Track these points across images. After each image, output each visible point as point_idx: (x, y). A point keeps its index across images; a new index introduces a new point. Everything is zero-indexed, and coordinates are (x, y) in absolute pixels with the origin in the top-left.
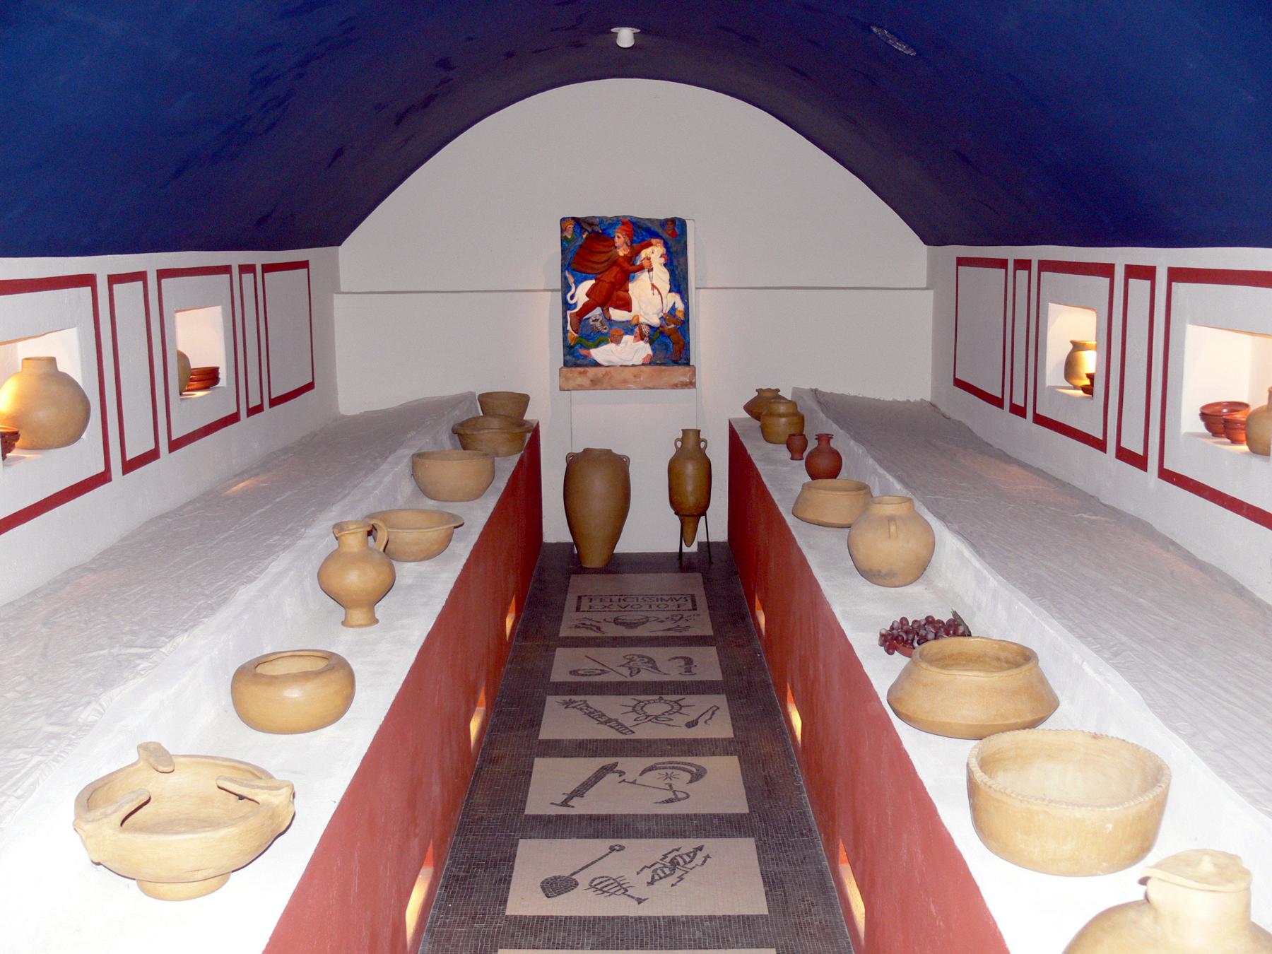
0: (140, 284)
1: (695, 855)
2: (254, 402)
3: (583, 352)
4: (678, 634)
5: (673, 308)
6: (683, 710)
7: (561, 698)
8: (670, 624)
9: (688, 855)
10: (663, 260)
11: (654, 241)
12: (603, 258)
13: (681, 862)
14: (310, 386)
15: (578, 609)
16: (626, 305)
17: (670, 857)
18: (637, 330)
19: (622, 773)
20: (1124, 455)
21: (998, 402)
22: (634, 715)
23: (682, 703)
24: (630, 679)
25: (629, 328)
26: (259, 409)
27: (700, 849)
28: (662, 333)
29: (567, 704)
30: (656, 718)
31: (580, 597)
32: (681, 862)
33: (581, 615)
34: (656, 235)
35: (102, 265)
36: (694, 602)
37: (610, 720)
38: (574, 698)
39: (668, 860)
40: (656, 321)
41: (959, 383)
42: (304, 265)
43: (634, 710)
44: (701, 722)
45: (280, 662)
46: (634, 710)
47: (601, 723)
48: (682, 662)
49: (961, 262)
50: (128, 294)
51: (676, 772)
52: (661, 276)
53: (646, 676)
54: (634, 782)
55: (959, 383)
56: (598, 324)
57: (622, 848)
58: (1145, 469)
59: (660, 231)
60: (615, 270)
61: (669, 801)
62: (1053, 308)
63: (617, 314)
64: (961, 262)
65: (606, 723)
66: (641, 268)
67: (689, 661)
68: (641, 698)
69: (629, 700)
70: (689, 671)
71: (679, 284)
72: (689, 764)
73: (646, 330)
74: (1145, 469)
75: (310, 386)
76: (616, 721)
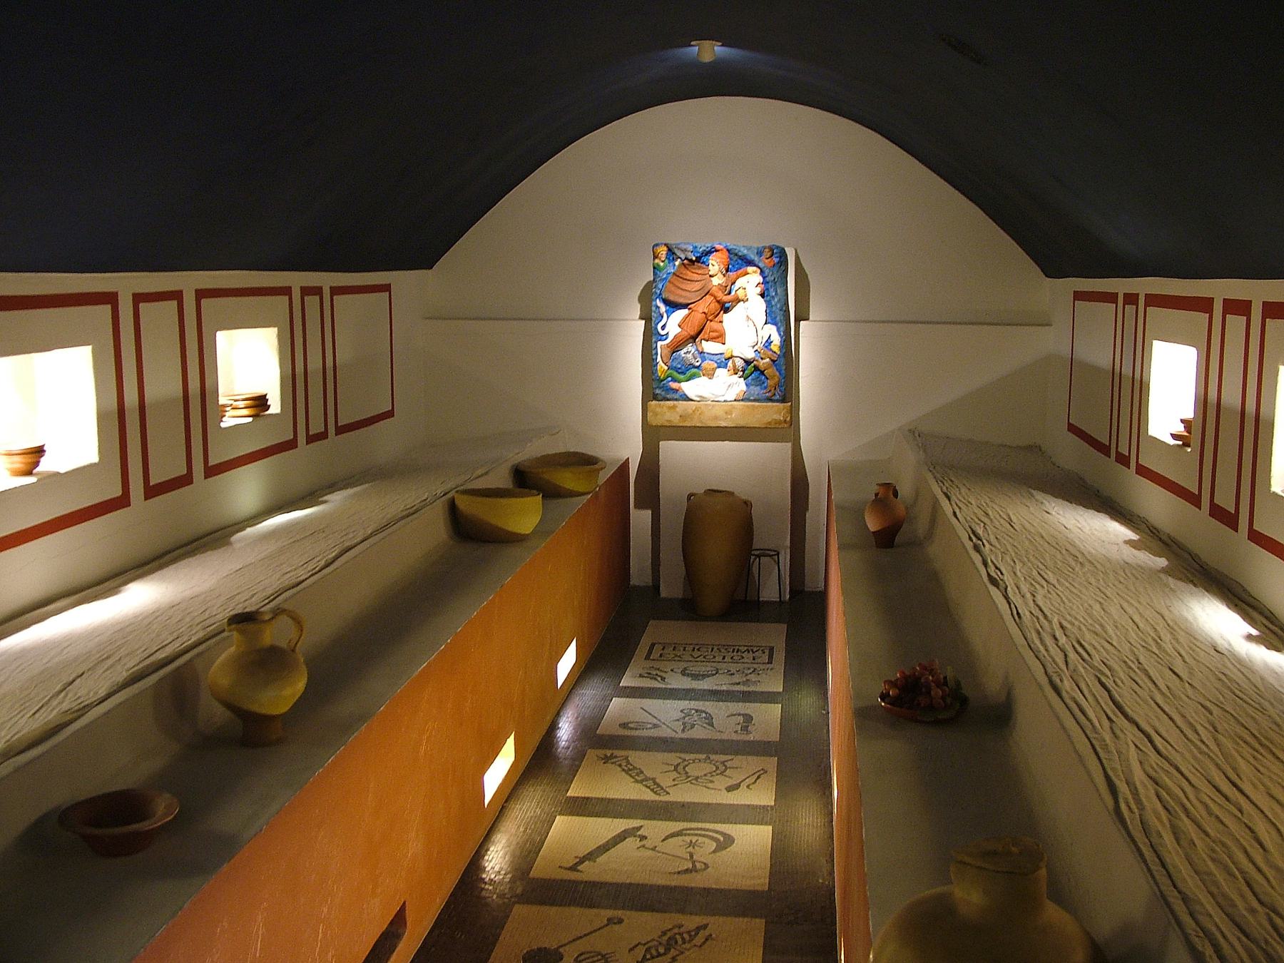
0: (107, 309)
1: (697, 934)
2: (316, 428)
3: (674, 385)
4: (746, 689)
5: (769, 342)
6: (727, 772)
7: (601, 752)
8: (737, 678)
9: (689, 932)
10: (759, 290)
11: (750, 269)
12: (697, 286)
13: (680, 942)
14: (389, 414)
15: (647, 658)
16: (720, 337)
17: (669, 934)
18: (730, 364)
19: (643, 838)
20: (1217, 512)
21: (1104, 449)
22: (675, 775)
23: (728, 764)
24: (683, 736)
25: (723, 361)
26: (323, 436)
27: (705, 927)
28: (756, 368)
29: (606, 759)
30: (697, 778)
31: (653, 645)
32: (680, 942)
33: (649, 664)
34: (750, 263)
35: (125, 283)
36: (771, 657)
37: (647, 779)
38: (616, 753)
39: (665, 938)
40: (750, 354)
41: (1072, 428)
42: (386, 288)
43: (676, 769)
44: (743, 785)
45: (102, 693)
46: (676, 769)
47: (637, 781)
48: (741, 719)
49: (1078, 296)
50: (159, 317)
51: (701, 839)
52: (755, 307)
53: (699, 733)
54: (654, 849)
55: (1072, 428)
56: (690, 356)
57: (620, 921)
58: (146, 499)
59: (753, 256)
60: (709, 299)
61: (687, 871)
62: (222, 337)
63: (710, 347)
64: (1078, 296)
65: (641, 782)
66: (738, 300)
67: (748, 718)
68: (687, 757)
69: (673, 758)
70: (745, 729)
71: (777, 315)
72: (717, 832)
73: (740, 363)
74: (146, 499)
75: (389, 414)
76: (654, 780)
